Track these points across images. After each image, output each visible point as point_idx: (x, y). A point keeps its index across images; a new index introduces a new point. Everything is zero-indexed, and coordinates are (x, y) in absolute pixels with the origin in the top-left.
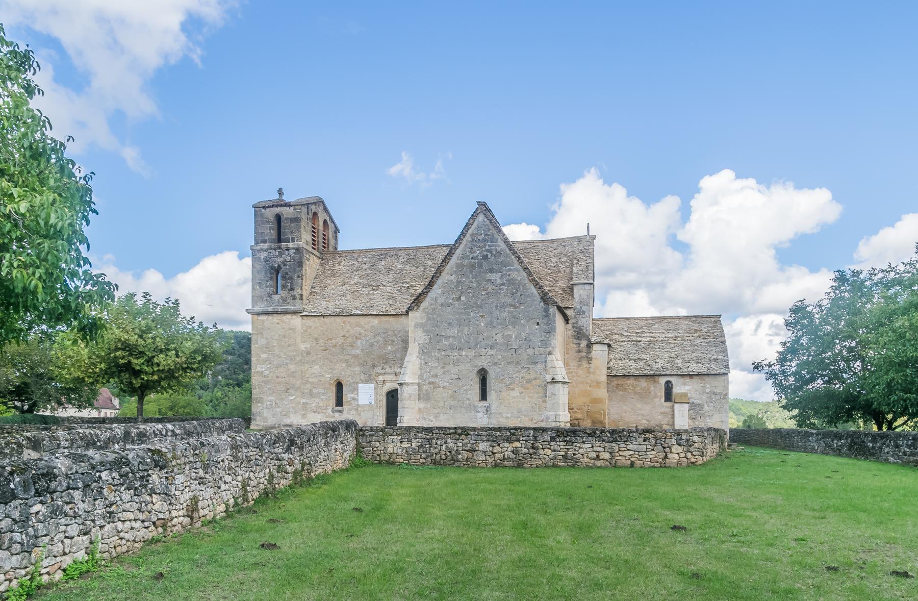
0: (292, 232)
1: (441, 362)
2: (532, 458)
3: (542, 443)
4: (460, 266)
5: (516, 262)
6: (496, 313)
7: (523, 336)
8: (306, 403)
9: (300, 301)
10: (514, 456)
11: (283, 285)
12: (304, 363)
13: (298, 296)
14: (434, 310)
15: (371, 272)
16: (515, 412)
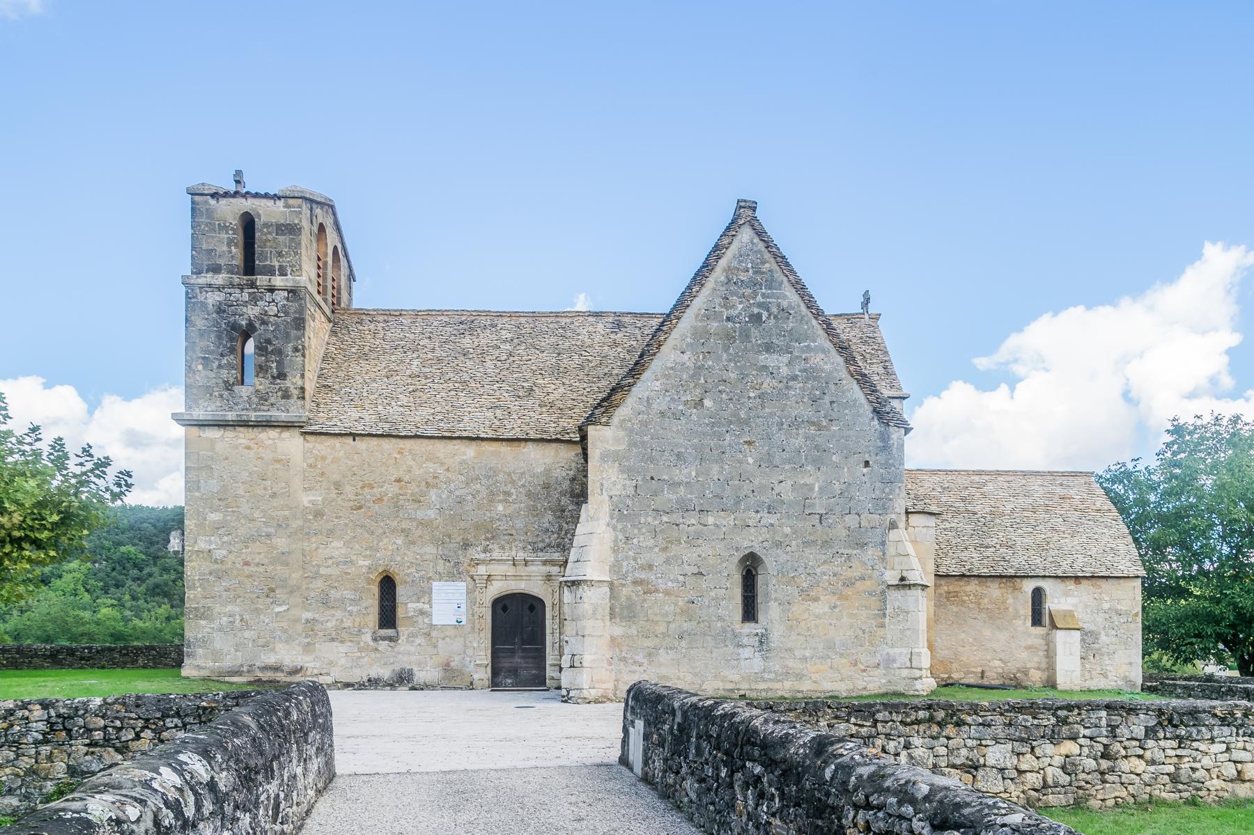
0: (280, 254)
1: (660, 537)
2: (1104, 782)
3: (1127, 743)
4: (701, 336)
5: (821, 332)
6: (779, 437)
7: (837, 487)
9: (300, 402)
10: (1068, 778)
11: (260, 367)
12: (307, 534)
14: (645, 424)
15: (445, 354)
16: (821, 646)
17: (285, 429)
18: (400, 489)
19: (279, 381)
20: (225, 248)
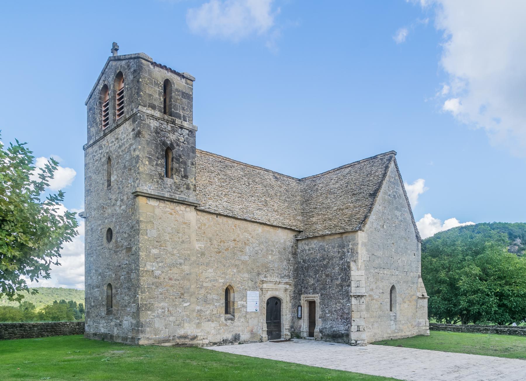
0: (183, 109)
12: (198, 264)
13: (192, 187)
17: (188, 206)
18: (235, 244)
19: (184, 179)
20: (157, 96)
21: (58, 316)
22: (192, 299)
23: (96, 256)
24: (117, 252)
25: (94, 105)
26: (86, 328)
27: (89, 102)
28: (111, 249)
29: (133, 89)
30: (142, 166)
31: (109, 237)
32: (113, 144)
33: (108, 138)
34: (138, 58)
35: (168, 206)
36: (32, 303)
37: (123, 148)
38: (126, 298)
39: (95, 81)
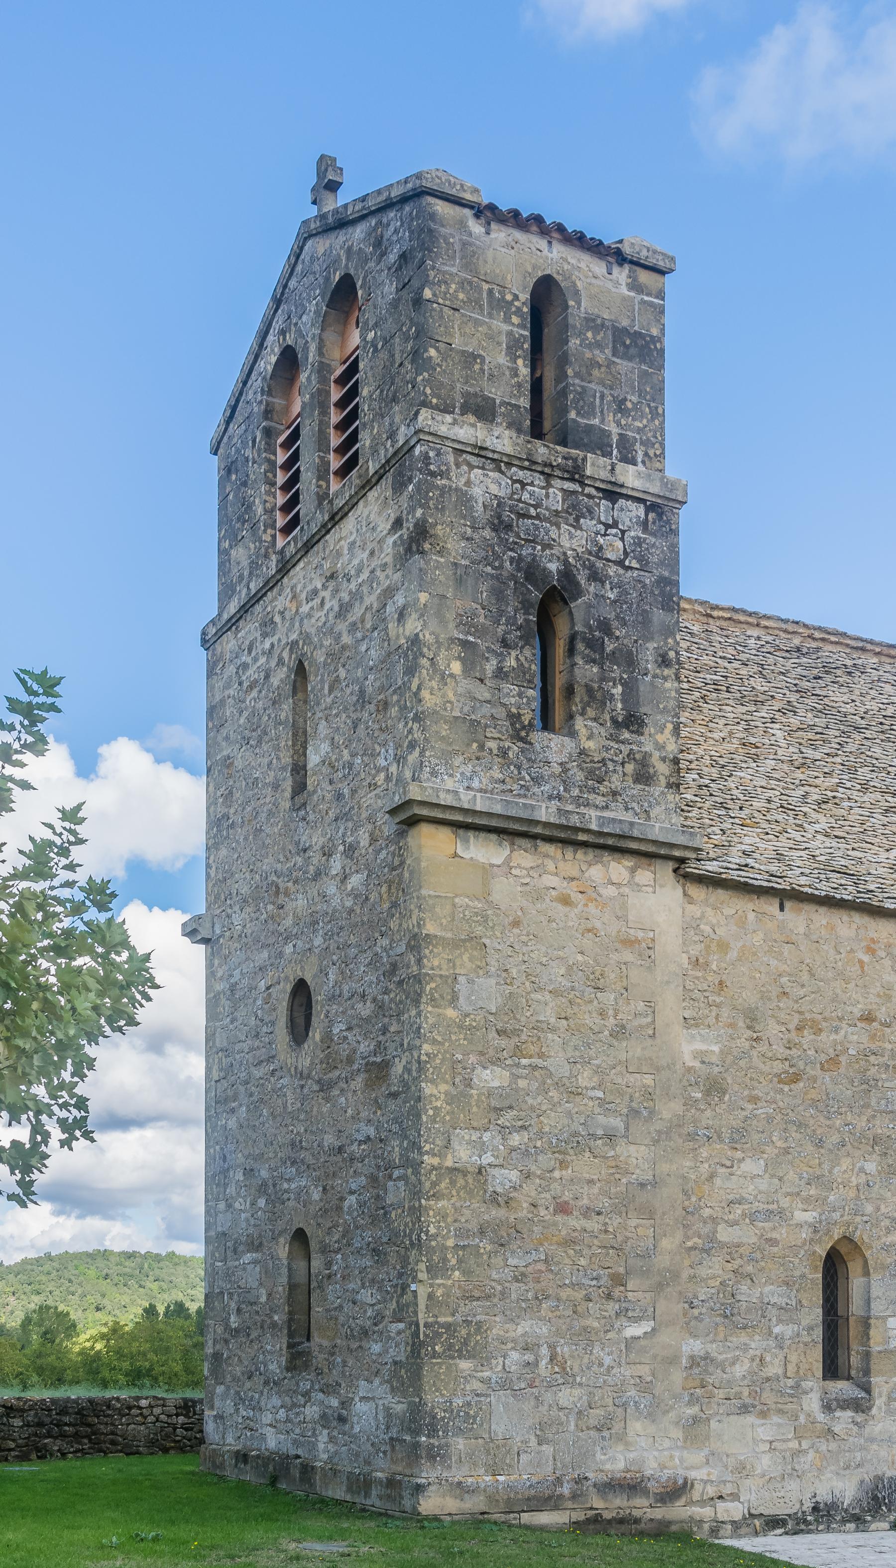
0: (620, 406)
8: (707, 1357)
12: (691, 1137)
13: (663, 769)
17: (644, 860)
18: (873, 1037)
19: (626, 735)
20: (502, 359)
21: (151, 1369)
22: (662, 1306)
23: (248, 1106)
24: (331, 1085)
25: (244, 444)
26: (210, 1427)
27: (225, 439)
28: (306, 1072)
29: (397, 340)
30: (434, 684)
31: (301, 1021)
32: (317, 601)
33: (294, 581)
34: (418, 194)
35: (551, 866)
36: (68, 1314)
37: (357, 611)
38: (367, 1296)
39: (249, 340)
